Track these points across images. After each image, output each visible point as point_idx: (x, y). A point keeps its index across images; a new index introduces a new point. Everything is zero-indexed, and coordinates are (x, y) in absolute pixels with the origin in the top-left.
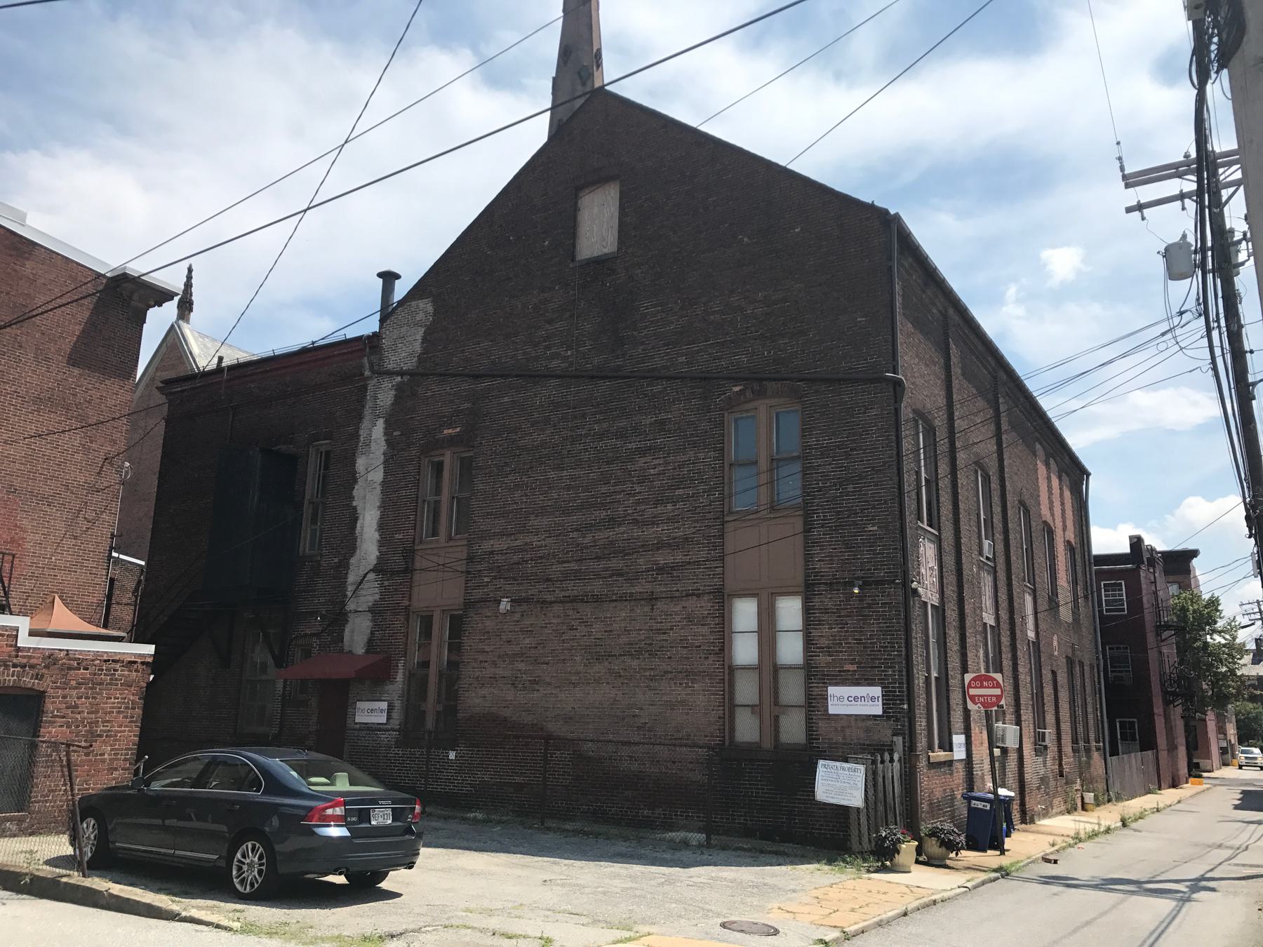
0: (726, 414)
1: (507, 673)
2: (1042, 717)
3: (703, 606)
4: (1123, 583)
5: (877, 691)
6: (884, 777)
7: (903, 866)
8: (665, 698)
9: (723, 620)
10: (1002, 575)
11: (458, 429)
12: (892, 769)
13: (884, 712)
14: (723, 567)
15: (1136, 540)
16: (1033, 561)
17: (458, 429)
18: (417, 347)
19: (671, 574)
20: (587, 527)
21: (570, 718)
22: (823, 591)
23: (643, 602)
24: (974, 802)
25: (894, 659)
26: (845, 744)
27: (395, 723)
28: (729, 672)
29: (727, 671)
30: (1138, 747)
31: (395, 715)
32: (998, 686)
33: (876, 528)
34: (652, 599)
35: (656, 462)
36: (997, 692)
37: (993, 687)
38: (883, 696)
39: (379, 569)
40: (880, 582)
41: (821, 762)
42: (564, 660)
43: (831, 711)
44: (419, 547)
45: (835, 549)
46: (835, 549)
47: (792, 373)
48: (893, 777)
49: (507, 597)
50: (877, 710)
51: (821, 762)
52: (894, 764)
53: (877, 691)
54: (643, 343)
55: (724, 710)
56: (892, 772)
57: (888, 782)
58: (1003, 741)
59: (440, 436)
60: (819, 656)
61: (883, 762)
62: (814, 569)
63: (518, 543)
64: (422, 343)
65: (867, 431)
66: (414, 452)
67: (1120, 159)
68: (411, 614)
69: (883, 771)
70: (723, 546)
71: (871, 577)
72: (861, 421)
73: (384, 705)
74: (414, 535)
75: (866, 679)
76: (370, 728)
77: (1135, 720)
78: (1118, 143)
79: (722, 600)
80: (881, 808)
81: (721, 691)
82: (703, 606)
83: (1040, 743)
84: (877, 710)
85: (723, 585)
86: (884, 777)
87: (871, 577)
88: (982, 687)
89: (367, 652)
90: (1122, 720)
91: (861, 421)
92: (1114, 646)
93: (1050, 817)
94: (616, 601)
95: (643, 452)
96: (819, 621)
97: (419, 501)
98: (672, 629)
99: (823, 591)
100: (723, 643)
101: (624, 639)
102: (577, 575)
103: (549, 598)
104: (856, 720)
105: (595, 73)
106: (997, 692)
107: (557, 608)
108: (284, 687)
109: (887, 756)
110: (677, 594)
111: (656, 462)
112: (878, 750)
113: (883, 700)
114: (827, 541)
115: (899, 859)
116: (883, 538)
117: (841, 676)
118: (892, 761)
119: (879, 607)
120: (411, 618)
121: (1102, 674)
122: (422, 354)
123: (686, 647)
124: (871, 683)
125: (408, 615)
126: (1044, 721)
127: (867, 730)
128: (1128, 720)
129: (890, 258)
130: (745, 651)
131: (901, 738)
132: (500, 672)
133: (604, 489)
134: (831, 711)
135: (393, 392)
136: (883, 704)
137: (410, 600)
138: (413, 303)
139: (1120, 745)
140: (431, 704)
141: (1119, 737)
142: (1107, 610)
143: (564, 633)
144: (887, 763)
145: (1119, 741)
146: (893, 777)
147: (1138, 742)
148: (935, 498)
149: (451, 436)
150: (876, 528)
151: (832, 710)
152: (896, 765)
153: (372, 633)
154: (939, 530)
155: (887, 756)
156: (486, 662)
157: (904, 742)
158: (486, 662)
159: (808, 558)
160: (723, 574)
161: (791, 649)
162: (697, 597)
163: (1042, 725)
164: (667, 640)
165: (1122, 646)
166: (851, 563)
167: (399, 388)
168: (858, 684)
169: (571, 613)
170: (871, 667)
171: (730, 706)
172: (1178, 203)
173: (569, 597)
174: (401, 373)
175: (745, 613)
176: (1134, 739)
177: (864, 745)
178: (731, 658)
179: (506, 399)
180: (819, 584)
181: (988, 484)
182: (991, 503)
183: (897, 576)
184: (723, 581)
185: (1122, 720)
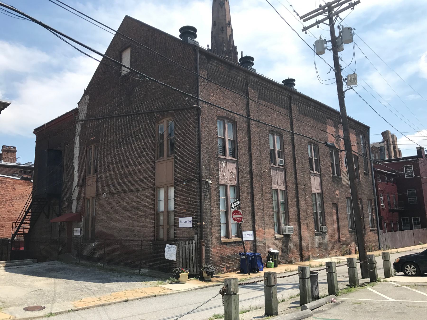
0: (156, 125)
1: (105, 218)
2: (324, 221)
3: (149, 192)
4: (412, 166)
5: (191, 219)
6: (189, 250)
7: (182, 281)
8: (141, 224)
9: (155, 197)
10: (290, 172)
11: (94, 137)
12: (192, 247)
13: (193, 226)
14: (155, 178)
15: (419, 149)
16: (320, 164)
17: (94, 137)
18: (86, 112)
19: (142, 182)
20: (188, 163)
21: (119, 232)
22: (178, 184)
23: (135, 192)
24: (242, 256)
25: (195, 207)
26: (183, 238)
27: (82, 234)
28: (157, 214)
29: (156, 214)
30: (420, 227)
31: (82, 232)
32: (241, 214)
33: (191, 161)
34: (138, 191)
35: (139, 143)
36: (240, 216)
37: (239, 215)
38: (193, 220)
39: (78, 185)
40: (192, 180)
41: (167, 245)
42: (118, 212)
43: (180, 227)
44: (88, 177)
45: (182, 169)
46: (182, 169)
47: (171, 108)
48: (192, 249)
49: (105, 193)
50: (191, 225)
51: (167, 245)
52: (193, 244)
53: (191, 219)
54: (136, 102)
55: (154, 227)
56: (192, 248)
57: (191, 251)
58: (285, 232)
59: (90, 140)
60: (177, 207)
61: (189, 244)
62: (176, 177)
63: (107, 174)
64: (87, 110)
65: (190, 126)
66: (85, 146)
67: (295, 11)
68: (85, 199)
69: (189, 247)
70: (155, 171)
71: (190, 178)
72: (188, 123)
73: (79, 229)
74: (85, 174)
75: (189, 215)
76: (77, 237)
77: (419, 217)
78: (291, 6)
79: (155, 189)
80: (188, 260)
81: (153, 221)
82: (149, 192)
83: (321, 231)
84: (191, 225)
85: (155, 184)
86: (189, 250)
87: (190, 178)
88: (236, 215)
89: (76, 212)
90: (403, 218)
91: (188, 123)
92: (410, 190)
93: (326, 258)
94: (129, 192)
95: (136, 140)
96: (177, 195)
97: (87, 162)
98: (142, 201)
99: (178, 184)
100: (155, 204)
101: (131, 205)
102: (120, 184)
103: (114, 192)
104: (186, 229)
105: (225, 3)
106: (240, 216)
107: (116, 195)
108: (60, 224)
109: (191, 242)
110: (143, 189)
111: (139, 143)
112: (191, 240)
113: (193, 222)
114: (180, 167)
115: (180, 279)
116: (193, 164)
117: (183, 214)
118: (192, 243)
119: (192, 189)
120: (85, 200)
121: (377, 202)
122: (87, 113)
123: (146, 207)
124: (190, 217)
125: (85, 200)
126: (325, 222)
127: (189, 233)
128: (416, 217)
129: (196, 63)
130: (161, 207)
131: (196, 235)
132: (103, 217)
133: (126, 154)
134: (180, 227)
135: (81, 127)
136: (193, 223)
137: (85, 195)
138: (85, 97)
139: (413, 227)
140: (90, 229)
141: (402, 225)
142: (406, 176)
143: (118, 204)
144: (191, 245)
145: (413, 225)
146: (192, 249)
147: (420, 225)
148: (236, 147)
149: (93, 140)
150: (191, 161)
151: (180, 226)
152: (194, 245)
153: (77, 206)
154: (238, 158)
155: (191, 242)
156: (101, 214)
157: (197, 237)
158: (101, 214)
159: (175, 173)
160: (155, 181)
161: (172, 206)
162: (148, 189)
163: (324, 224)
164: (141, 205)
165: (413, 190)
166: (185, 174)
167: (82, 125)
168: (186, 217)
169: (119, 197)
170: (190, 210)
171: (157, 225)
172: (316, 26)
173: (119, 191)
174: (82, 121)
175: (162, 194)
176: (418, 224)
177: (188, 238)
178: (157, 209)
179: (105, 126)
180: (177, 182)
181: (282, 138)
182: (283, 145)
183: (196, 178)
184: (155, 183)
185: (403, 218)
